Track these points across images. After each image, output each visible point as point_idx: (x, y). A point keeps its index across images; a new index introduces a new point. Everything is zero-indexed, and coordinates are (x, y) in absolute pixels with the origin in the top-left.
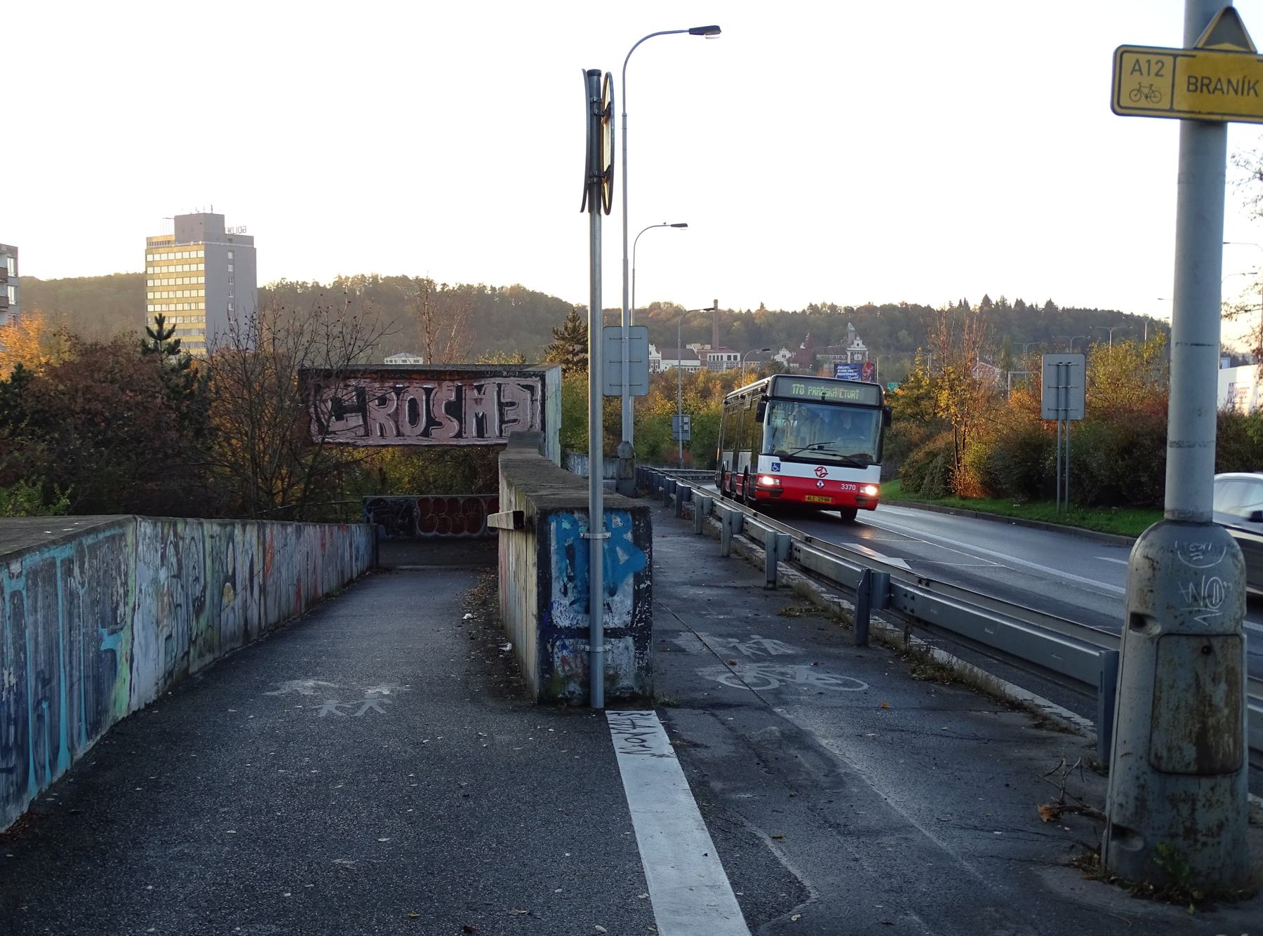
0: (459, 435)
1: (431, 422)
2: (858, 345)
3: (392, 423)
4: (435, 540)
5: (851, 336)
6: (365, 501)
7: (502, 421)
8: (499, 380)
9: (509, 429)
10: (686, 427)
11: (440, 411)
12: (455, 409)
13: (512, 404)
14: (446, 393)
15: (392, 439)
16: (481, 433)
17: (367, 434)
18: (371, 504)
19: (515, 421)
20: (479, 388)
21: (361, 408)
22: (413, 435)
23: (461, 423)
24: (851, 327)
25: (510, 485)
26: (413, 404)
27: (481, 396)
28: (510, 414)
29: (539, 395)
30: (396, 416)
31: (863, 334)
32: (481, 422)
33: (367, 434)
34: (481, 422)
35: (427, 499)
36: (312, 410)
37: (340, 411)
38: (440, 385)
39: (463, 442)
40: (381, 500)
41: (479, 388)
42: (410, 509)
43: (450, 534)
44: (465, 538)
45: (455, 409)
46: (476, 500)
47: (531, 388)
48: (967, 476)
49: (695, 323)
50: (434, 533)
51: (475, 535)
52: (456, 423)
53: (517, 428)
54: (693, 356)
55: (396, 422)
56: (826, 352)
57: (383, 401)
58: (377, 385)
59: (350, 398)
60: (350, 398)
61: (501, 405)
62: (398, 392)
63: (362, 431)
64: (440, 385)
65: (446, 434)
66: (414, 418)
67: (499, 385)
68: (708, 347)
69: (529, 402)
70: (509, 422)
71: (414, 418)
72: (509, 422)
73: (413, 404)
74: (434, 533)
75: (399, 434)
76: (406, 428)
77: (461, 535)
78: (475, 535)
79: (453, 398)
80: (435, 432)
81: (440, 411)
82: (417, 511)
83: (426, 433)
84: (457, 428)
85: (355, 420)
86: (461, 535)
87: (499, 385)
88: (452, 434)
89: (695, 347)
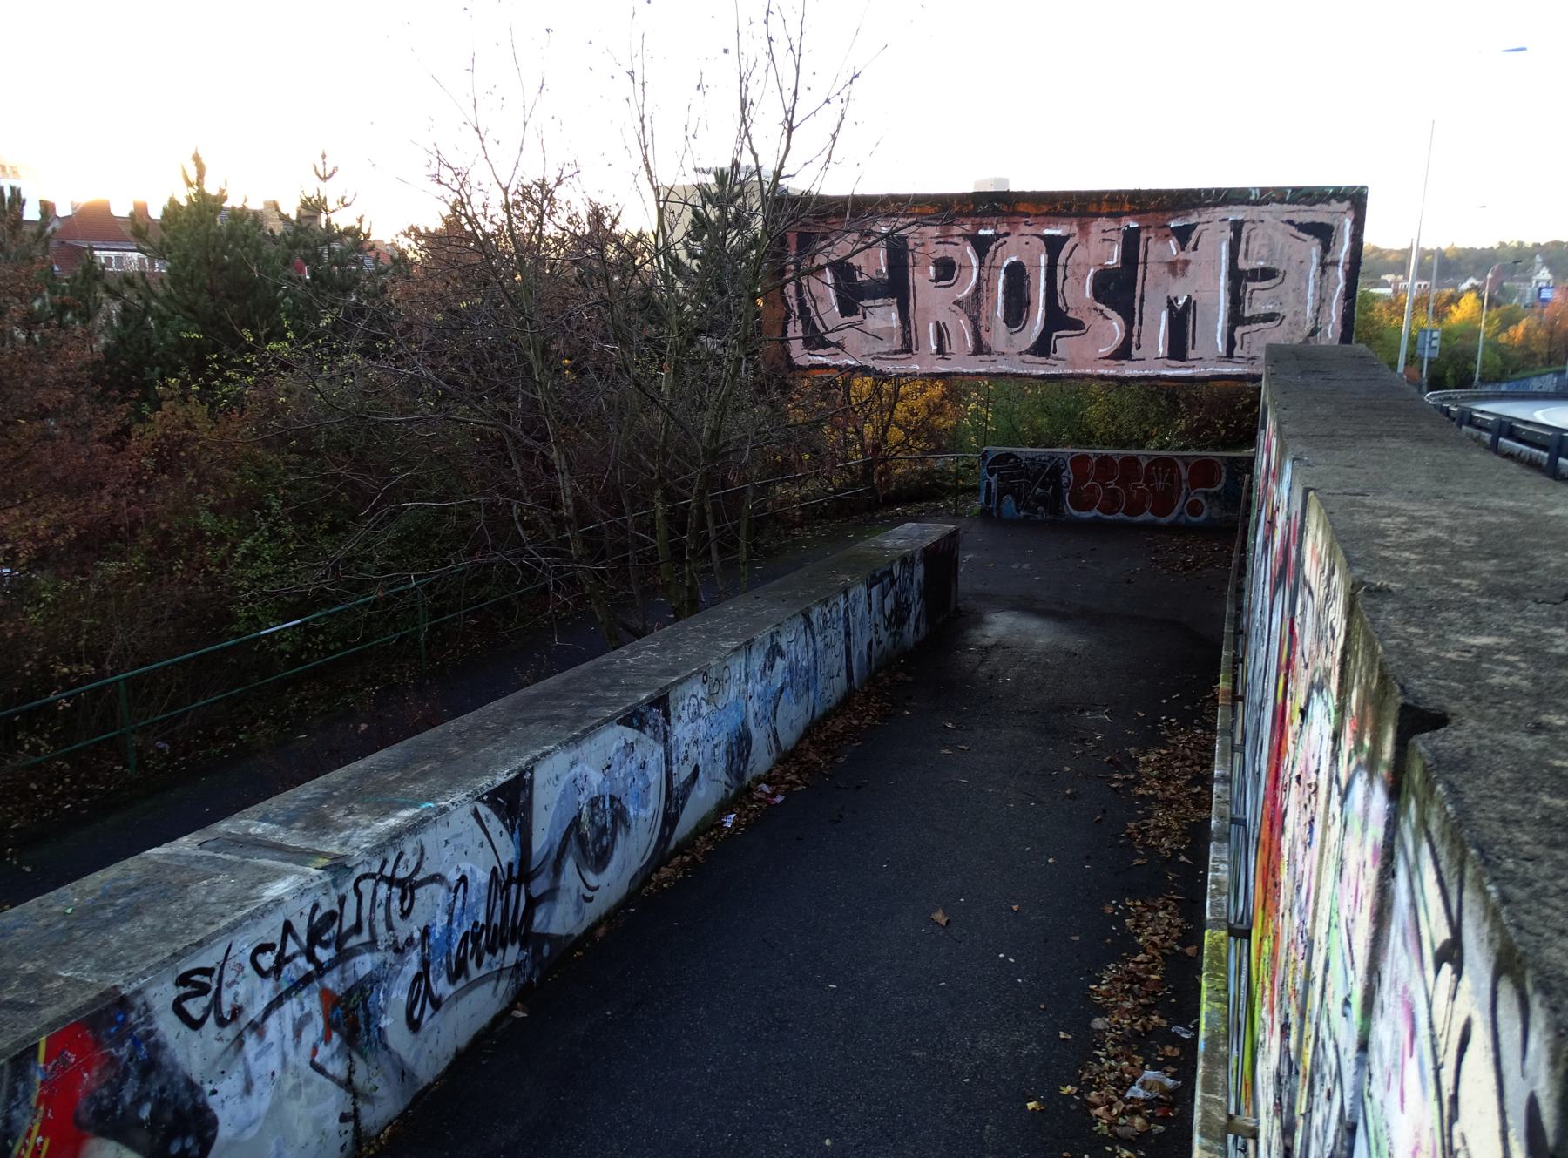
0: (1123, 352)
1: (1058, 319)
2: (1544, 275)
3: (964, 323)
4: (1096, 524)
5: (1537, 266)
6: (984, 456)
7: (1236, 318)
8: (1236, 213)
9: (1256, 340)
10: (1435, 343)
11: (1079, 294)
12: (1117, 289)
13: (1267, 274)
14: (1100, 248)
15: (962, 362)
16: (1178, 348)
17: (907, 348)
18: (994, 462)
19: (1270, 317)
20: (1183, 235)
21: (897, 287)
22: (1011, 351)
23: (1129, 323)
24: (1538, 258)
25: (1411, 730)
26: (1017, 276)
27: (1191, 255)
28: (1259, 300)
29: (1343, 252)
30: (973, 306)
31: (1549, 264)
32: (1181, 322)
33: (907, 348)
34: (1181, 322)
35: (1086, 457)
36: (791, 289)
37: (852, 296)
38: (1084, 229)
39: (1130, 370)
40: (1010, 455)
41: (1183, 235)
42: (1056, 472)
43: (1120, 515)
44: (1144, 526)
45: (1117, 289)
46: (1169, 463)
47: (1324, 233)
48: (1449, 380)
49: (1390, 258)
50: (1095, 512)
51: (1163, 520)
52: (1117, 325)
53: (1276, 335)
54: (1387, 285)
55: (975, 322)
56: (1512, 280)
57: (946, 270)
58: (934, 231)
59: (873, 264)
60: (873, 264)
61: (1238, 278)
62: (981, 245)
63: (897, 343)
64: (1084, 229)
65: (1091, 350)
66: (1016, 311)
67: (1237, 226)
68: (1401, 277)
69: (1314, 268)
70: (1254, 320)
71: (1016, 311)
72: (1254, 320)
73: (1017, 276)
74: (1095, 512)
75: (980, 348)
76: (998, 334)
77: (1139, 518)
78: (1163, 520)
79: (1114, 261)
80: (1064, 344)
81: (1079, 294)
82: (1068, 475)
83: (1043, 347)
84: (1119, 335)
85: (883, 316)
86: (1139, 518)
87: (1237, 226)
88: (1105, 350)
89: (1389, 278)
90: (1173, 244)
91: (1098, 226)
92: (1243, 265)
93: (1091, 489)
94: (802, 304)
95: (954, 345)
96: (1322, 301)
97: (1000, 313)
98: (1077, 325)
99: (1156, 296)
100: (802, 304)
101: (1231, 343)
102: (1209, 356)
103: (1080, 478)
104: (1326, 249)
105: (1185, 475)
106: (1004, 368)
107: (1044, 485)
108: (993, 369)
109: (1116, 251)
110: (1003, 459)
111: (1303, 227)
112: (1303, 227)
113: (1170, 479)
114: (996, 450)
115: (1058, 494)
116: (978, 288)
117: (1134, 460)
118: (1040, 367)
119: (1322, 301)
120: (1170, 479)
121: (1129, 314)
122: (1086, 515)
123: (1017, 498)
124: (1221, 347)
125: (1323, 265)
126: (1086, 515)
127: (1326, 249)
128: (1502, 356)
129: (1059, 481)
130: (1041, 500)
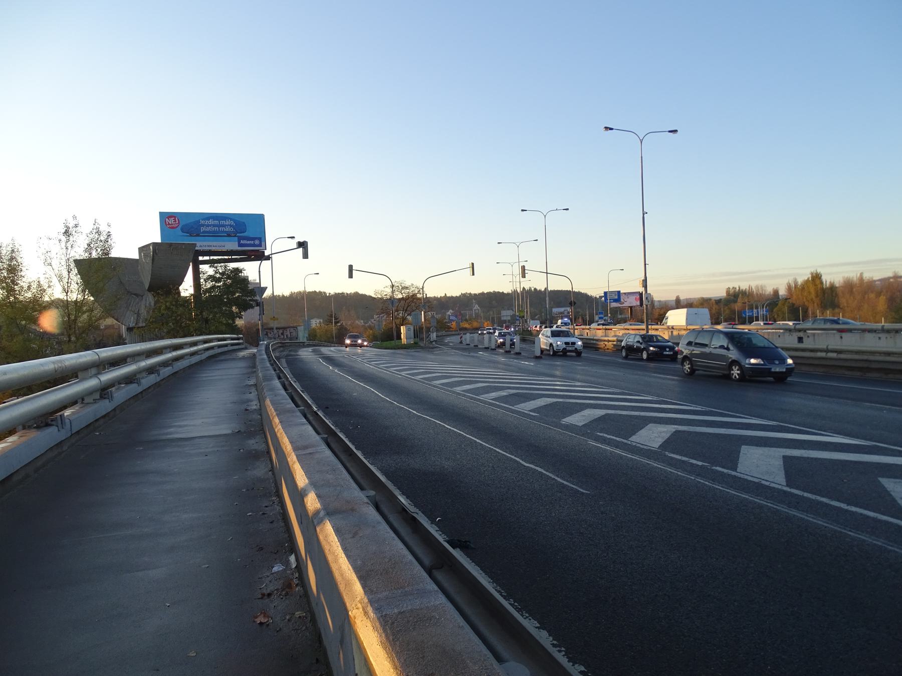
12: (282, 334)
14: (281, 331)
45: (282, 334)
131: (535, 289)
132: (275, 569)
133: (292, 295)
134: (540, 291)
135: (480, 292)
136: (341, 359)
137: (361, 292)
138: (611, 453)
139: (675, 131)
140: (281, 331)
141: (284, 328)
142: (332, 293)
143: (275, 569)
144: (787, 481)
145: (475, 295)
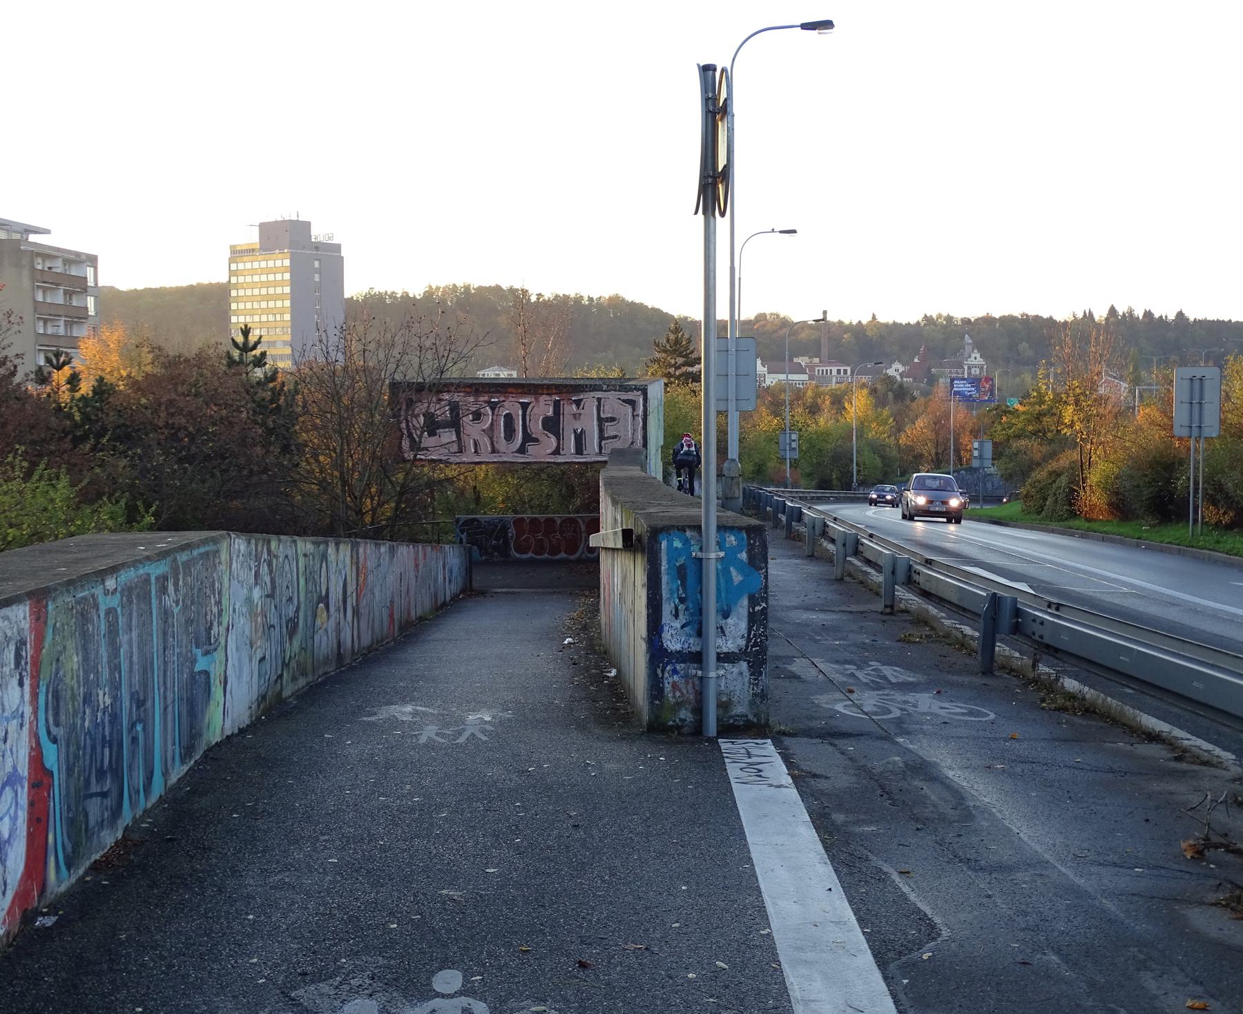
0: (557, 452)
1: (528, 438)
3: (486, 439)
4: (531, 562)
8: (599, 394)
9: (609, 445)
10: (794, 445)
11: (537, 427)
12: (553, 425)
13: (613, 419)
14: (543, 408)
16: (579, 451)
19: (615, 437)
20: (578, 403)
21: (455, 424)
22: (508, 452)
23: (558, 440)
24: (968, 339)
26: (509, 419)
28: (610, 430)
30: (490, 432)
31: (980, 346)
32: (580, 438)
34: (580, 438)
36: (403, 425)
37: (432, 427)
38: (537, 399)
39: (560, 459)
40: (474, 520)
41: (578, 403)
42: (504, 529)
43: (546, 556)
45: (553, 425)
47: (632, 403)
48: (835, 482)
50: (530, 555)
51: (572, 557)
52: (553, 440)
53: (617, 444)
55: (491, 438)
56: (941, 366)
57: (477, 416)
58: (471, 399)
59: (442, 412)
60: (442, 412)
61: (600, 420)
62: (493, 407)
63: (455, 448)
65: (542, 451)
66: (510, 433)
67: (599, 400)
68: (816, 360)
69: (630, 417)
71: (510, 433)
73: (509, 419)
74: (530, 555)
75: (494, 451)
76: (502, 444)
77: (558, 557)
78: (572, 557)
79: (550, 413)
81: (537, 427)
82: (512, 532)
83: (522, 450)
84: (555, 444)
85: (448, 436)
86: (558, 557)
87: (599, 400)
88: (549, 451)
89: (803, 361)
90: (574, 406)
91: (543, 398)
92: (602, 416)
93: (527, 540)
94: (408, 430)
95: (482, 449)
96: (634, 430)
97: (502, 435)
98: (536, 440)
99: (569, 427)
100: (408, 430)
101: (600, 448)
102: (592, 452)
103: (519, 533)
104: (634, 410)
105: (583, 528)
106: (506, 459)
107: (497, 539)
108: (501, 460)
109: (551, 409)
110: (467, 522)
111: (624, 401)
112: (624, 401)
113: (575, 531)
114: (464, 517)
115: (506, 543)
116: (492, 424)
117: (552, 520)
118: (521, 459)
119: (634, 430)
120: (575, 531)
121: (557, 435)
122: (525, 556)
123: (480, 548)
124: (597, 450)
125: (633, 416)
126: (525, 556)
127: (634, 410)
128: (883, 457)
129: (506, 534)
130: (496, 548)
131: (1148, 314)
132: (690, 975)
133: (429, 295)
134: (1162, 321)
135: (981, 314)
136: (1099, 595)
137: (630, 297)
138: (984, 707)
139: (827, 25)
140: (543, 408)
141: (570, 390)
142: (548, 295)
143: (690, 975)
144: (597, 561)
145: (966, 321)
